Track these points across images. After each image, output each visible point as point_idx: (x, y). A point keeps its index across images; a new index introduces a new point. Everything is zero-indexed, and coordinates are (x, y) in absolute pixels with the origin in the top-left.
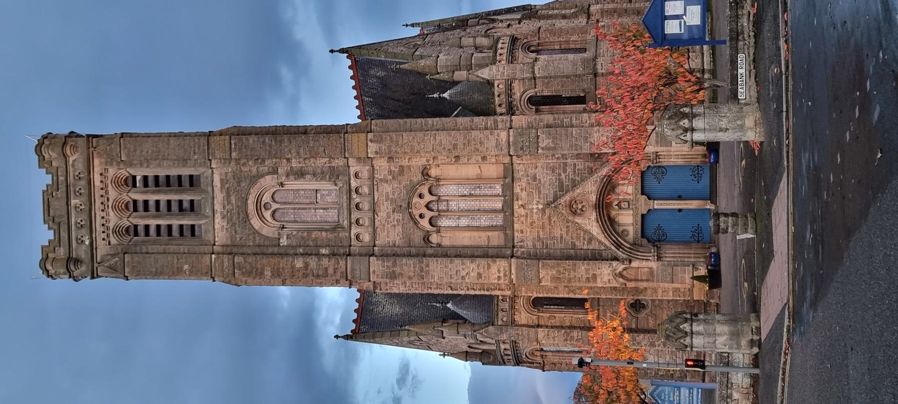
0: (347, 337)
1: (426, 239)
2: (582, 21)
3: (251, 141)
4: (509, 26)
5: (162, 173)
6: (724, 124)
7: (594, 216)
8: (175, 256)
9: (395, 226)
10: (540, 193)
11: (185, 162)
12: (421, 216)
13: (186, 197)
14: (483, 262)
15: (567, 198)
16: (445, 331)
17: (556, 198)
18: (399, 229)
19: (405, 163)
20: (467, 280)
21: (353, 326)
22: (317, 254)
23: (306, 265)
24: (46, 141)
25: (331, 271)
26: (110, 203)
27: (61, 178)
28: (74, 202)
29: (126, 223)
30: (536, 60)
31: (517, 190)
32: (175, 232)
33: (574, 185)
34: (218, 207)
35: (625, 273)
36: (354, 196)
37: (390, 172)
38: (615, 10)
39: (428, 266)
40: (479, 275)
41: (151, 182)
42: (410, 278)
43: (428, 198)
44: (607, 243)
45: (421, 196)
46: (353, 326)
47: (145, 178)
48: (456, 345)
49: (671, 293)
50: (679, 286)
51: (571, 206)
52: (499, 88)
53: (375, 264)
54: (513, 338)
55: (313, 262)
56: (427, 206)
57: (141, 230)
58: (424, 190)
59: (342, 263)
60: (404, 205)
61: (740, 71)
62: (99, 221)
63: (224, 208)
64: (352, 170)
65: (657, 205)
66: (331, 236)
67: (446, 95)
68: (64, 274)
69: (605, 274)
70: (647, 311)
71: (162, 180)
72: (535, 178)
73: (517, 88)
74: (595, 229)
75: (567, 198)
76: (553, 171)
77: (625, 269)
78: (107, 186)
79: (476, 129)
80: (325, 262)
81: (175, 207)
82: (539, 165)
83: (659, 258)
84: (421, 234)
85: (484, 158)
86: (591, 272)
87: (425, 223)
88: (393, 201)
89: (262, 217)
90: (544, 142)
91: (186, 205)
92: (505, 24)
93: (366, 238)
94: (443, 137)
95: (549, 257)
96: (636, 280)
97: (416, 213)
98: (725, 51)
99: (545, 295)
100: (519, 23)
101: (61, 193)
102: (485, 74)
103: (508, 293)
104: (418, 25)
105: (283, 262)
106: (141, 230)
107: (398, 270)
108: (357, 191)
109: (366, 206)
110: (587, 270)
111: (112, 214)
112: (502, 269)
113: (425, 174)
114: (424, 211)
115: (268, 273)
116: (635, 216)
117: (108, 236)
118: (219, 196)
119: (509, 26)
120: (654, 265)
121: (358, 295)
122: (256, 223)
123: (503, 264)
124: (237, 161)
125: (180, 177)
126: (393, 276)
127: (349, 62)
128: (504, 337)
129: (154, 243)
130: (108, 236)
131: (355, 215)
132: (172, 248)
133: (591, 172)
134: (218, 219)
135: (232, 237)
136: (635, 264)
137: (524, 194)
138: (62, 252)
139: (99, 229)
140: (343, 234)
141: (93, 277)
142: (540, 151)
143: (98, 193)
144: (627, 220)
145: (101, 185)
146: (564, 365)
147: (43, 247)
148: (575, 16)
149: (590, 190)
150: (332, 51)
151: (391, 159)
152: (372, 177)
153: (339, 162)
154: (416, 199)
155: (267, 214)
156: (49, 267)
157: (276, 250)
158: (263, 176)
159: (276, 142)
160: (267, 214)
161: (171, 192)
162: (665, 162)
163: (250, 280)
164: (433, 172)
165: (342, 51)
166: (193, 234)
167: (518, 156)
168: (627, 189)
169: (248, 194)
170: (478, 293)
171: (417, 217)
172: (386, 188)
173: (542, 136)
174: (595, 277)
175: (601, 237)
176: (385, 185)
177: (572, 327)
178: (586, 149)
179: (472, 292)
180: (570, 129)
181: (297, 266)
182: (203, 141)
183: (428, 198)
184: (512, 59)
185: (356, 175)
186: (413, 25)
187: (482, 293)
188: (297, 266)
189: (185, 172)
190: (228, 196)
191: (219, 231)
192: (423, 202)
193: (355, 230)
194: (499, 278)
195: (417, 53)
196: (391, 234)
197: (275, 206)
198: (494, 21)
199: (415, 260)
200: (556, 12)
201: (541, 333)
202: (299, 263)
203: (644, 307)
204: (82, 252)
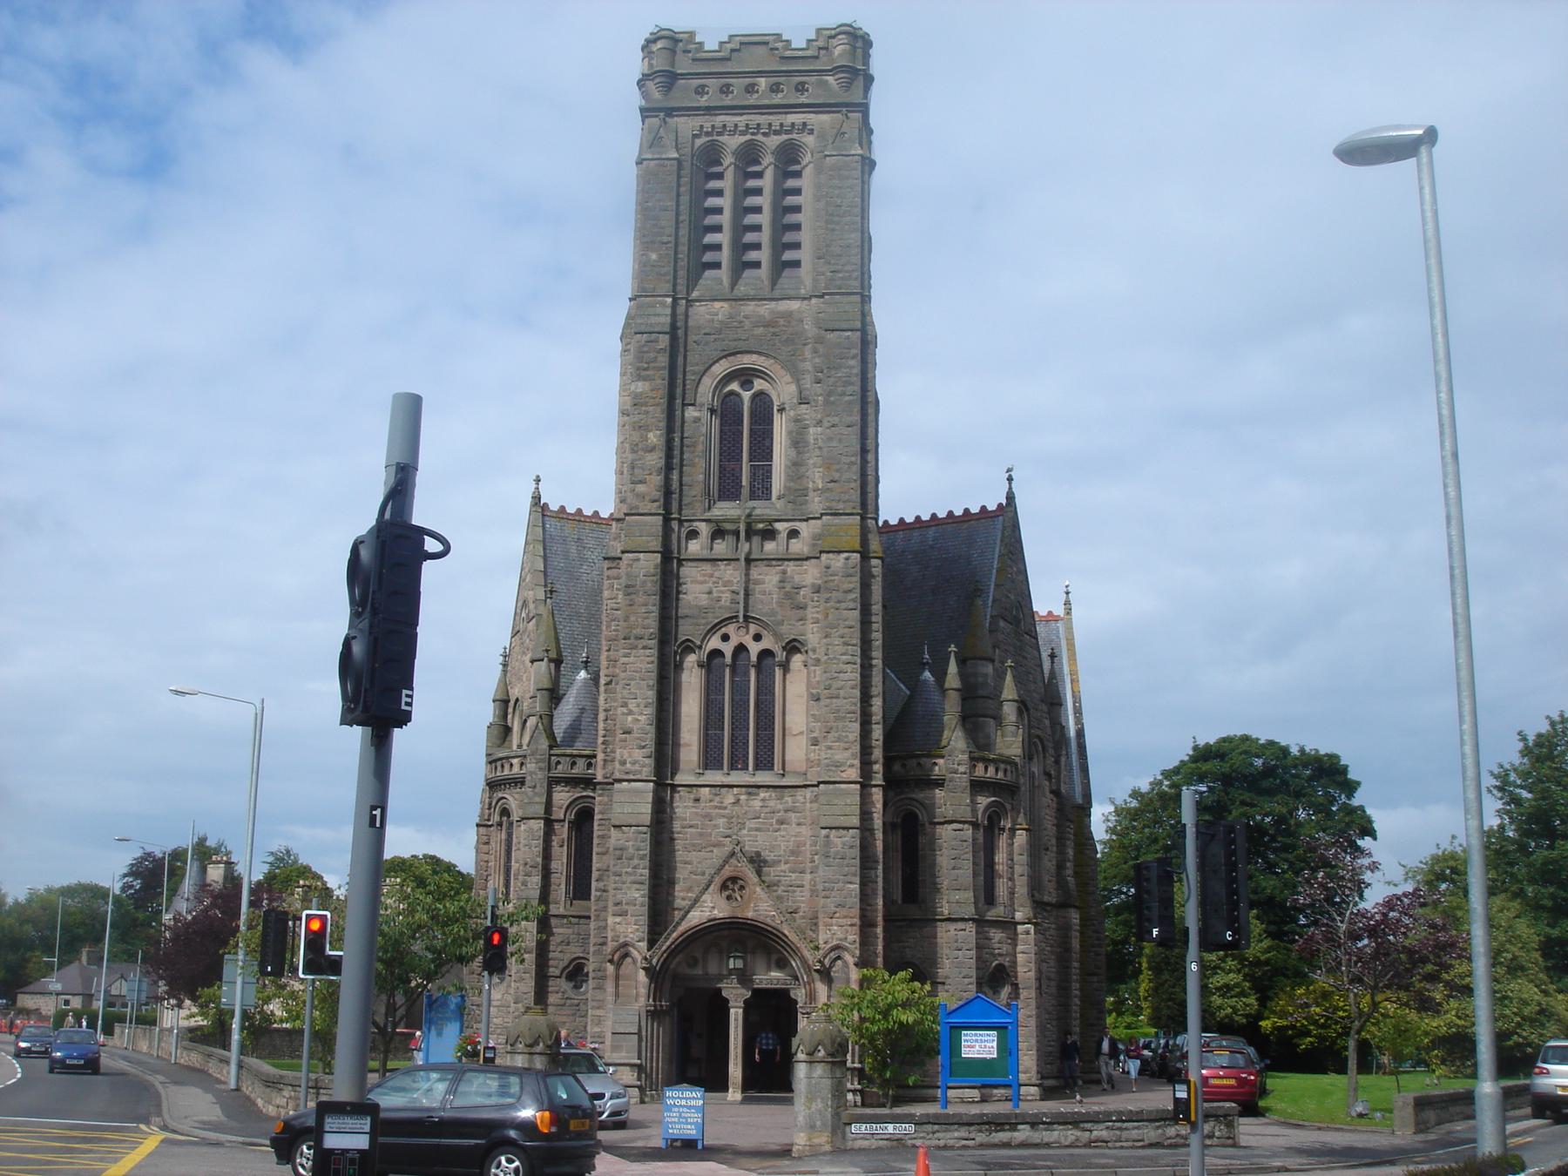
0: (537, 498)
3: (852, 362)
4: (1048, 775)
7: (717, 913)
8: (672, 239)
9: (710, 593)
10: (757, 830)
12: (725, 638)
16: (544, 664)
18: (704, 600)
19: (811, 613)
20: (620, 710)
21: (554, 507)
23: (652, 449)
24: (859, 42)
25: (641, 488)
26: (759, 137)
28: (763, 82)
31: (763, 794)
34: (750, 308)
35: (629, 960)
38: (1068, 950)
39: (644, 648)
42: (626, 619)
43: (754, 649)
44: (674, 935)
46: (554, 507)
48: (520, 679)
49: (597, 1029)
50: (608, 1042)
51: (734, 879)
54: (528, 778)
56: (741, 649)
58: (766, 643)
61: (890, 1126)
63: (746, 317)
64: (802, 527)
67: (927, 674)
68: (651, 65)
69: (630, 928)
70: (570, 993)
72: (781, 822)
74: (697, 917)
75: (750, 874)
76: (793, 853)
77: (634, 961)
78: (787, 132)
82: (803, 829)
86: (630, 909)
87: (714, 643)
91: (753, 255)
93: (694, 547)
96: (617, 978)
97: (730, 629)
99: (595, 834)
100: (1052, 792)
103: (599, 778)
104: (1068, 612)
107: (640, 599)
110: (632, 903)
111: (743, 139)
112: (637, 767)
113: (793, 647)
115: (640, 387)
117: (708, 134)
119: (1048, 775)
121: (605, 514)
126: (629, 589)
127: (992, 507)
128: (531, 766)
130: (708, 134)
135: (699, 328)
139: (720, 119)
141: (642, 110)
142: (824, 832)
143: (776, 120)
145: (730, 127)
146: (486, 857)
147: (692, 34)
148: (1061, 883)
150: (538, 480)
153: (816, 504)
155: (734, 386)
156: (660, 45)
158: (797, 381)
159: (850, 402)
160: (734, 386)
163: (630, 357)
165: (1010, 497)
167: (815, 799)
170: (601, 725)
171: (724, 630)
174: (623, 914)
176: (776, 578)
179: (601, 716)
180: (857, 880)
181: (651, 435)
183: (754, 649)
185: (794, 534)
186: (1067, 603)
187: (601, 732)
188: (651, 435)
189: (805, 255)
190: (767, 325)
192: (748, 641)
194: (623, 763)
195: (1002, 623)
203: (577, 987)
204: (683, 95)
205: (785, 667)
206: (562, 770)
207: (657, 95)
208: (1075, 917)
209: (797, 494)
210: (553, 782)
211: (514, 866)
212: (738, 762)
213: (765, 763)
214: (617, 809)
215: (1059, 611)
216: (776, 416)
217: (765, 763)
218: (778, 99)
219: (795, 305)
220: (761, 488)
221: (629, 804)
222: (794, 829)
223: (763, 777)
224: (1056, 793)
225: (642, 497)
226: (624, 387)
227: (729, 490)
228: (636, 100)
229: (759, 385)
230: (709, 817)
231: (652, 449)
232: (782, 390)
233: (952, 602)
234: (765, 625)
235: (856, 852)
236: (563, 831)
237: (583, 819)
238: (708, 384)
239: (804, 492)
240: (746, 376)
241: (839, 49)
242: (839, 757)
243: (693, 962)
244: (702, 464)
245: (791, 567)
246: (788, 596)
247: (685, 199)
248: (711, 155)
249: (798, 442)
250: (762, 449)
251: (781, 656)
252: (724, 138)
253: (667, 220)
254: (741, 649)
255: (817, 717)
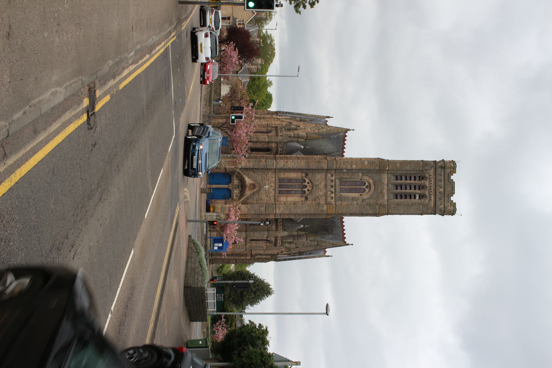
0: (349, 130)
1: (307, 175)
2: (254, 252)
5: (408, 200)
6: (209, 217)
11: (398, 204)
12: (308, 183)
13: (399, 191)
14: (285, 167)
15: (256, 190)
17: (260, 189)
18: (317, 178)
19: (314, 202)
21: (347, 134)
22: (347, 170)
23: (351, 166)
24: (453, 212)
25: (342, 164)
27: (446, 199)
28: (442, 190)
29: (422, 182)
30: (267, 237)
31: (273, 192)
32: (403, 178)
33: (253, 194)
34: (386, 187)
36: (333, 191)
37: (319, 199)
38: (241, 256)
40: (287, 162)
41: (413, 197)
43: (306, 190)
45: (308, 190)
46: (347, 134)
47: (415, 198)
51: (255, 186)
52: (280, 228)
53: (325, 167)
55: (349, 167)
56: (306, 187)
57: (417, 178)
58: (307, 192)
59: (338, 166)
60: (314, 187)
62: (433, 182)
64: (334, 200)
65: (226, 186)
66: (343, 176)
67: (302, 226)
69: (244, 163)
71: (408, 197)
72: (267, 196)
73: (274, 227)
75: (256, 190)
79: (287, 214)
80: (344, 167)
81: (403, 187)
83: (226, 169)
84: (308, 176)
85: (285, 203)
87: (307, 181)
88: (318, 189)
89: (369, 183)
90: (263, 209)
91: (399, 188)
92: (283, 253)
93: (329, 175)
94: (299, 212)
95: (263, 169)
97: (310, 184)
98: (209, 236)
101: (447, 193)
102: (286, 233)
103: (277, 156)
104: (327, 256)
105: (360, 167)
106: (417, 178)
107: (317, 164)
108: (332, 192)
109: (329, 187)
111: (428, 185)
113: (306, 198)
114: (307, 185)
115: (366, 163)
116: (233, 183)
118: (385, 191)
120: (228, 167)
122: (371, 181)
123: (278, 167)
124: (377, 204)
125: (401, 198)
126: (319, 162)
127: (346, 240)
128: (280, 138)
129: (412, 174)
131: (333, 184)
132: (404, 172)
133: (248, 198)
134: (386, 183)
136: (234, 167)
137: (271, 190)
138: (448, 171)
139: (433, 180)
140: (338, 177)
143: (432, 193)
144: (236, 182)
148: (256, 255)
149: (248, 193)
151: (319, 204)
152: (326, 197)
153: (339, 203)
154: (310, 189)
155: (367, 184)
156: (452, 165)
157: (363, 171)
158: (368, 199)
161: (404, 193)
162: (223, 201)
164: (304, 199)
165: (348, 245)
166: (397, 177)
167: (272, 204)
168: (236, 192)
169: (374, 192)
172: (321, 193)
173: (264, 211)
175: (244, 176)
177: (256, 142)
178: (249, 206)
182: (390, 212)
183: (306, 190)
184: (276, 238)
185: (332, 198)
186: (329, 256)
189: (399, 200)
191: (385, 178)
193: (333, 178)
196: (319, 177)
197: (364, 187)
198: (289, 254)
199: (310, 168)
200: (264, 257)
201: (267, 140)
202: (354, 167)
204: (439, 171)
205: (302, 196)
206: (280, 145)
207: (439, 165)
208: (249, 258)
209: (341, 199)
210: (277, 143)
211: (258, 134)
212: (280, 186)
213: (280, 192)
214: (270, 160)
215: (327, 254)
216: (359, 194)
217: (280, 192)
218: (438, 194)
219: (386, 198)
220: (342, 191)
221: (271, 163)
222: (266, 198)
223: (277, 192)
224: (278, 254)
225: (340, 164)
226: (366, 159)
227: (342, 182)
228: (438, 160)
229: (367, 190)
230: (268, 180)
231: (351, 166)
232: (365, 196)
233: (319, 233)
234: (311, 192)
235: (260, 213)
236: (266, 146)
237: (268, 150)
238: (367, 178)
239: (342, 201)
240: (369, 187)
241: (451, 208)
242: (281, 209)
243: (237, 177)
244: (349, 177)
245: (324, 198)
246: (318, 197)
247: (413, 172)
248: (422, 178)
249: (353, 199)
250: (351, 191)
251: (304, 196)
252: (428, 181)
253: (408, 168)
254: (306, 187)
255: (291, 204)
